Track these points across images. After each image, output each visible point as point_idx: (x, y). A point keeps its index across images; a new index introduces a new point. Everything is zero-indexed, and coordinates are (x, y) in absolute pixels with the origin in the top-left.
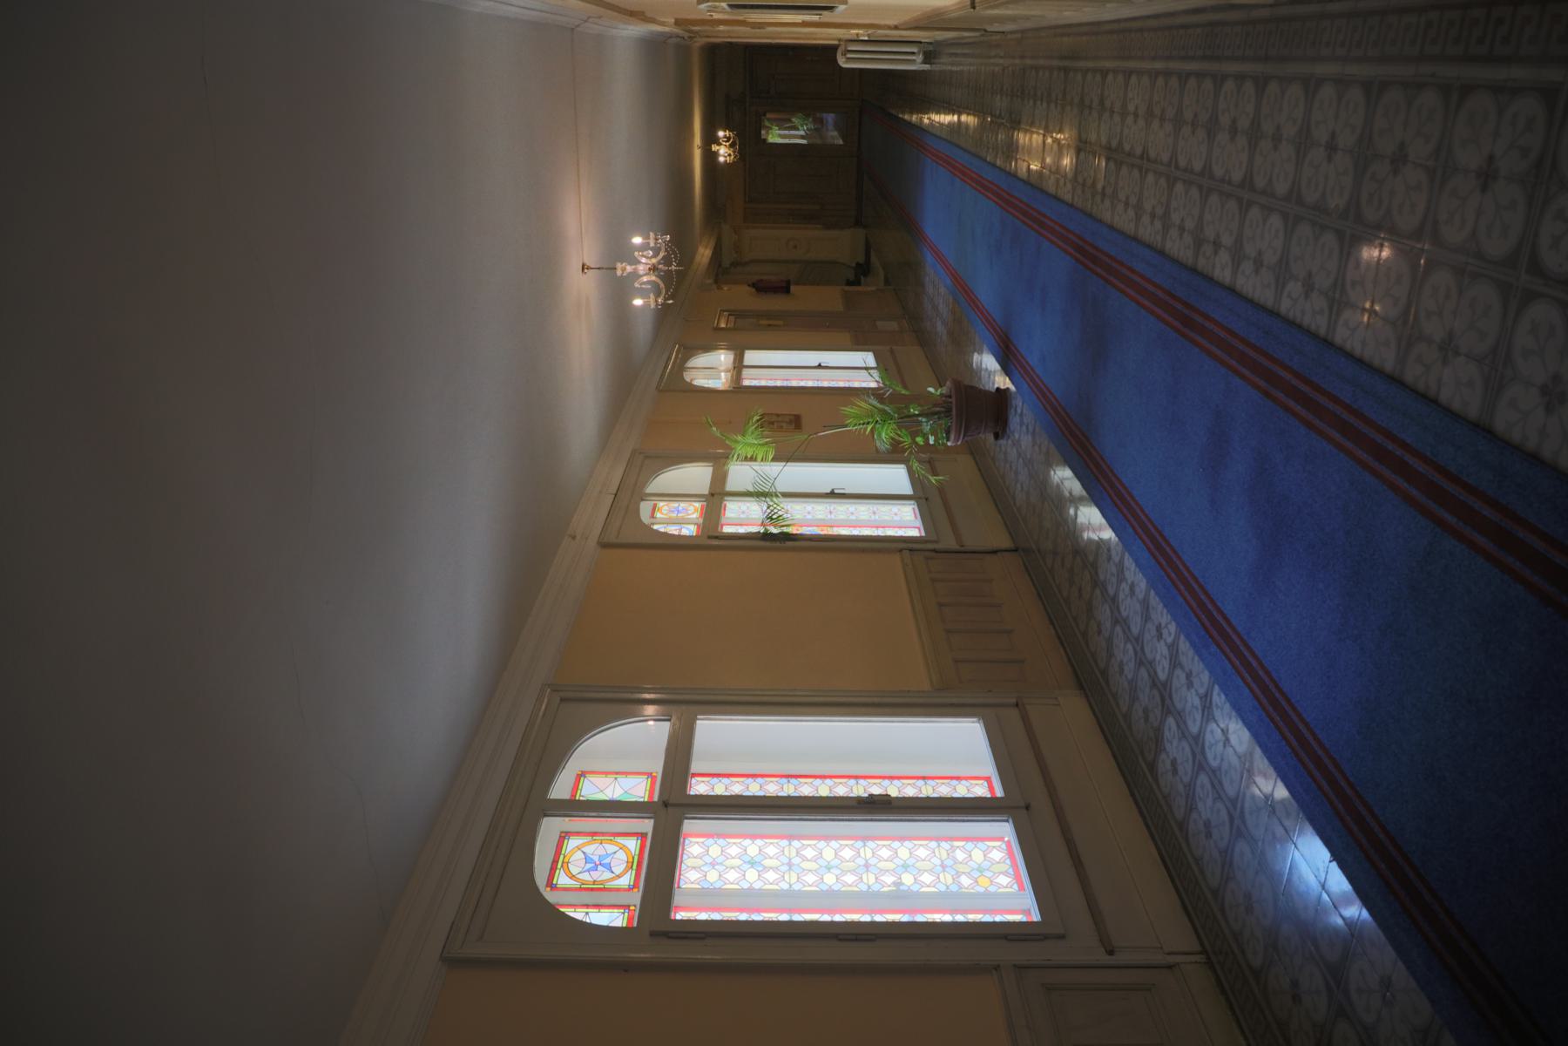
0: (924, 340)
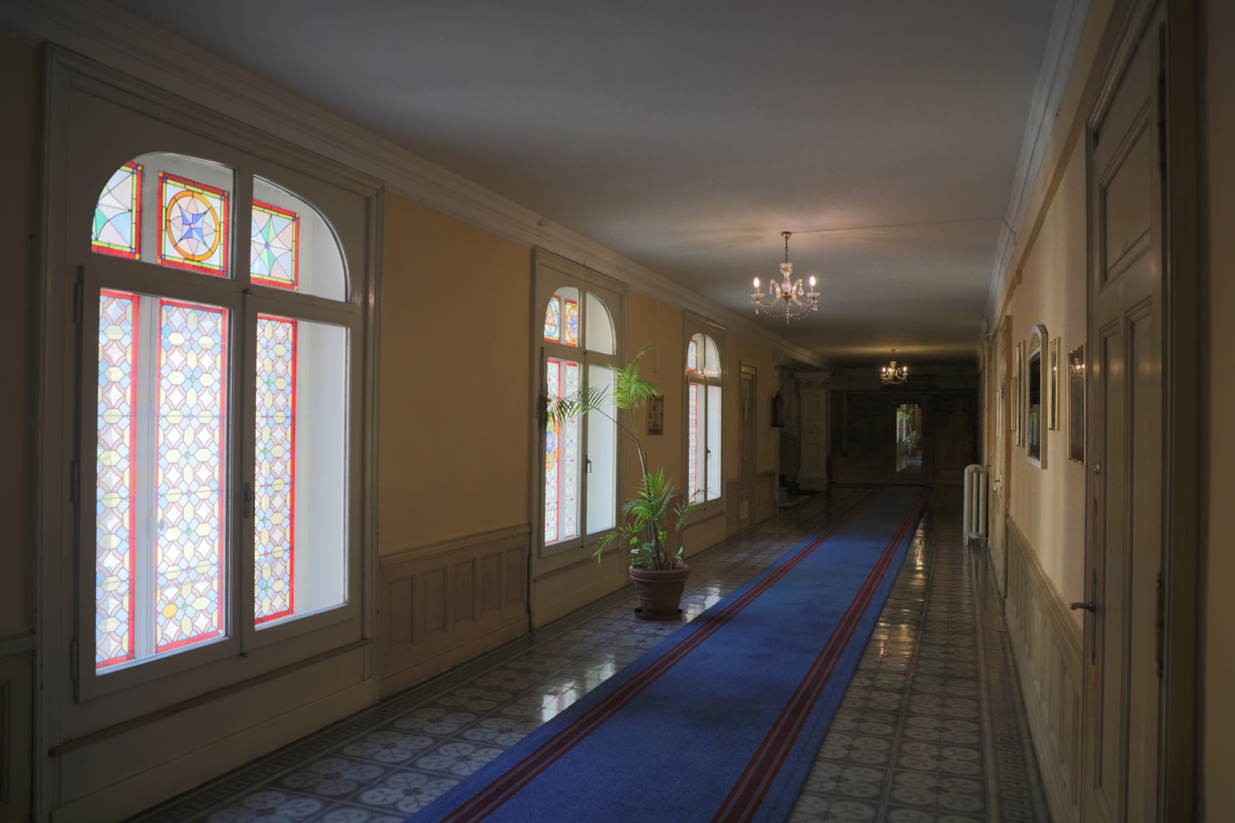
0: (732, 541)
